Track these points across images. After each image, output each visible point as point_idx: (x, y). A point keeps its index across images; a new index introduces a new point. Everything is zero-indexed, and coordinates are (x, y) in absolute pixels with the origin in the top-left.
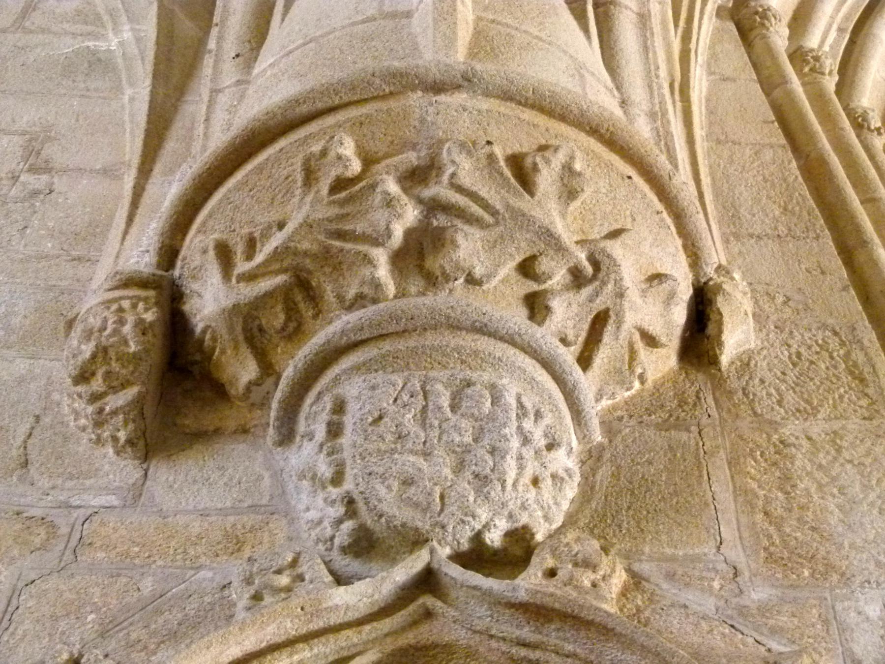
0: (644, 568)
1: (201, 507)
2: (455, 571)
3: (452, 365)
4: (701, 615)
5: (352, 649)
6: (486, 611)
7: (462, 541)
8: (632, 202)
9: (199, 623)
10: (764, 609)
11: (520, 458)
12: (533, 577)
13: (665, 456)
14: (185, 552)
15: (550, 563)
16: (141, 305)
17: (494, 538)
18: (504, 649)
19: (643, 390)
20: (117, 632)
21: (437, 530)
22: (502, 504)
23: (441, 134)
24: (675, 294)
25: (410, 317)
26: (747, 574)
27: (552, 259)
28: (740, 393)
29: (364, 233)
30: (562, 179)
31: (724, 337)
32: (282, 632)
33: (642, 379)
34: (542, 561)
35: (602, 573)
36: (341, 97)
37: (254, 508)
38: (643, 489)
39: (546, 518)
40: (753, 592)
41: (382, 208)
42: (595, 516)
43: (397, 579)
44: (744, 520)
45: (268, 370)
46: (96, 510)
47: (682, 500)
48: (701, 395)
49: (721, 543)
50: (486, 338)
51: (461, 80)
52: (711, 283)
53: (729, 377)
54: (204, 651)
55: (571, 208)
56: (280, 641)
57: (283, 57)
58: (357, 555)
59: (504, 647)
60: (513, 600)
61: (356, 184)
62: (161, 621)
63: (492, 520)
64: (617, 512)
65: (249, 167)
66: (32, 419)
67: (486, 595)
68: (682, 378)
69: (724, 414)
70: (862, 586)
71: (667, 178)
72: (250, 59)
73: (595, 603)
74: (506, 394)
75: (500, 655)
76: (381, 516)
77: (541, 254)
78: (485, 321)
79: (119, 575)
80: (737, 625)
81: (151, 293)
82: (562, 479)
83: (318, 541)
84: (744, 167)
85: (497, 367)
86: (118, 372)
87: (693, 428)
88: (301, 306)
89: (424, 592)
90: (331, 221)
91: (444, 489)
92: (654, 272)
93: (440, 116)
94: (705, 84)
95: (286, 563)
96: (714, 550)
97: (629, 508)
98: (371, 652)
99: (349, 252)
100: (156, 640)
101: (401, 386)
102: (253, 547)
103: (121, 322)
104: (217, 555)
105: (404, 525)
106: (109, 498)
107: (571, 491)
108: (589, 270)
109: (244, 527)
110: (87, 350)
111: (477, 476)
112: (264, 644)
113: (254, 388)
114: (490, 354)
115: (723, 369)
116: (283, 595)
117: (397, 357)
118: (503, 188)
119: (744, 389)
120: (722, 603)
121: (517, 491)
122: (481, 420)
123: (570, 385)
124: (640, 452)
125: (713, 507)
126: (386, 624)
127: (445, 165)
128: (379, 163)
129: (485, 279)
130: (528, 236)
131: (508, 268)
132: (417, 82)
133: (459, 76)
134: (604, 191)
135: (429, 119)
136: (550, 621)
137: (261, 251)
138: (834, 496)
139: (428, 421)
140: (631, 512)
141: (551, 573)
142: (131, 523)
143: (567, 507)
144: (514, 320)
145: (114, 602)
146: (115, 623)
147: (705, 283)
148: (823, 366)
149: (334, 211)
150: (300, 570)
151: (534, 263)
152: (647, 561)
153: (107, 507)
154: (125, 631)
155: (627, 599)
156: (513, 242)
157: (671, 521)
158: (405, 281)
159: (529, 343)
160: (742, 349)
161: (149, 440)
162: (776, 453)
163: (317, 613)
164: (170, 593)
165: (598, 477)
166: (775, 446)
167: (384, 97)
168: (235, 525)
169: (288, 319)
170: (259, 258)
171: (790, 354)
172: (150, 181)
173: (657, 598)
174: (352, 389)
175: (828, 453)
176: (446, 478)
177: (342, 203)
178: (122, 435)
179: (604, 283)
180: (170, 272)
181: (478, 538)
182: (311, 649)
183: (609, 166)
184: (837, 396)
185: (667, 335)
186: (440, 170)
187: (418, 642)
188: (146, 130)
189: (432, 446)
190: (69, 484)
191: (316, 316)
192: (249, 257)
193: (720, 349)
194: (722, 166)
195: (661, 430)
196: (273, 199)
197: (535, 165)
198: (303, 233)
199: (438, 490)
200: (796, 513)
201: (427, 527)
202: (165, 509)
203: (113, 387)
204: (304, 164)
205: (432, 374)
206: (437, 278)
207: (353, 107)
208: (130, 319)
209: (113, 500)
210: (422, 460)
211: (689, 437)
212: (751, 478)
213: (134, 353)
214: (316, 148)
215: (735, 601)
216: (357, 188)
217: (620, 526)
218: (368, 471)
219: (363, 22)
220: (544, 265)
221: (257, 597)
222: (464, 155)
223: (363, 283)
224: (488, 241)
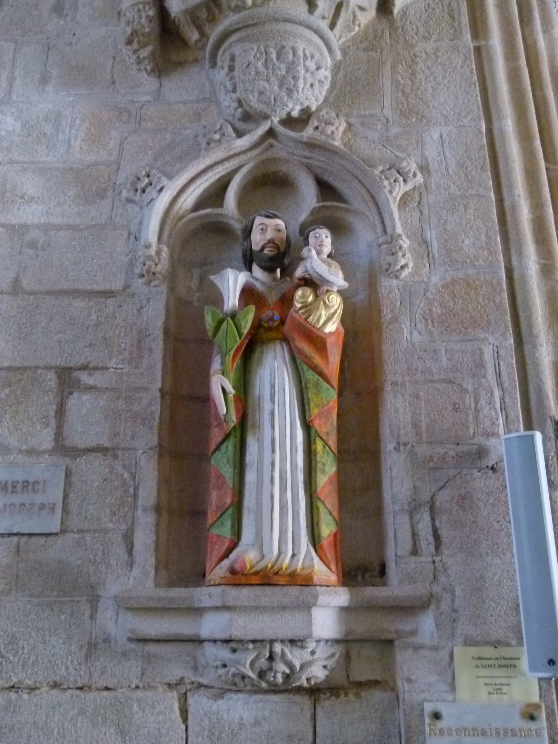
0: (353, 120)
2: (280, 129)
11: (305, 78)
14: (180, 121)
15: (316, 123)
16: (147, 7)
17: (295, 114)
19: (359, 31)
26: (391, 121)
28: (401, 29)
33: (359, 26)
34: (314, 122)
35: (335, 126)
37: (203, 100)
38: (356, 83)
39: (316, 100)
44: (394, 95)
45: (203, 35)
59: (299, 158)
66: (112, 59)
70: (434, 125)
73: (331, 142)
80: (385, 145)
83: (229, 116)
88: (213, 8)
96: (380, 112)
97: (349, 92)
103: (140, 17)
105: (260, 111)
107: (327, 86)
110: (129, 30)
111: (287, 89)
112: (213, 162)
116: (217, 144)
119: (402, 27)
123: (326, 39)
138: (431, 82)
141: (317, 128)
145: (157, 145)
148: (438, 11)
165: (338, 77)
169: (209, 15)
171: (425, 5)
174: (237, 50)
175: (432, 59)
178: (149, 68)
181: (289, 114)
184: (441, 28)
189: (270, 77)
190: (132, 91)
199: (273, 96)
200: (414, 92)
205: (269, 44)
208: (144, 15)
210: (266, 83)
212: (400, 75)
221: (208, 143)
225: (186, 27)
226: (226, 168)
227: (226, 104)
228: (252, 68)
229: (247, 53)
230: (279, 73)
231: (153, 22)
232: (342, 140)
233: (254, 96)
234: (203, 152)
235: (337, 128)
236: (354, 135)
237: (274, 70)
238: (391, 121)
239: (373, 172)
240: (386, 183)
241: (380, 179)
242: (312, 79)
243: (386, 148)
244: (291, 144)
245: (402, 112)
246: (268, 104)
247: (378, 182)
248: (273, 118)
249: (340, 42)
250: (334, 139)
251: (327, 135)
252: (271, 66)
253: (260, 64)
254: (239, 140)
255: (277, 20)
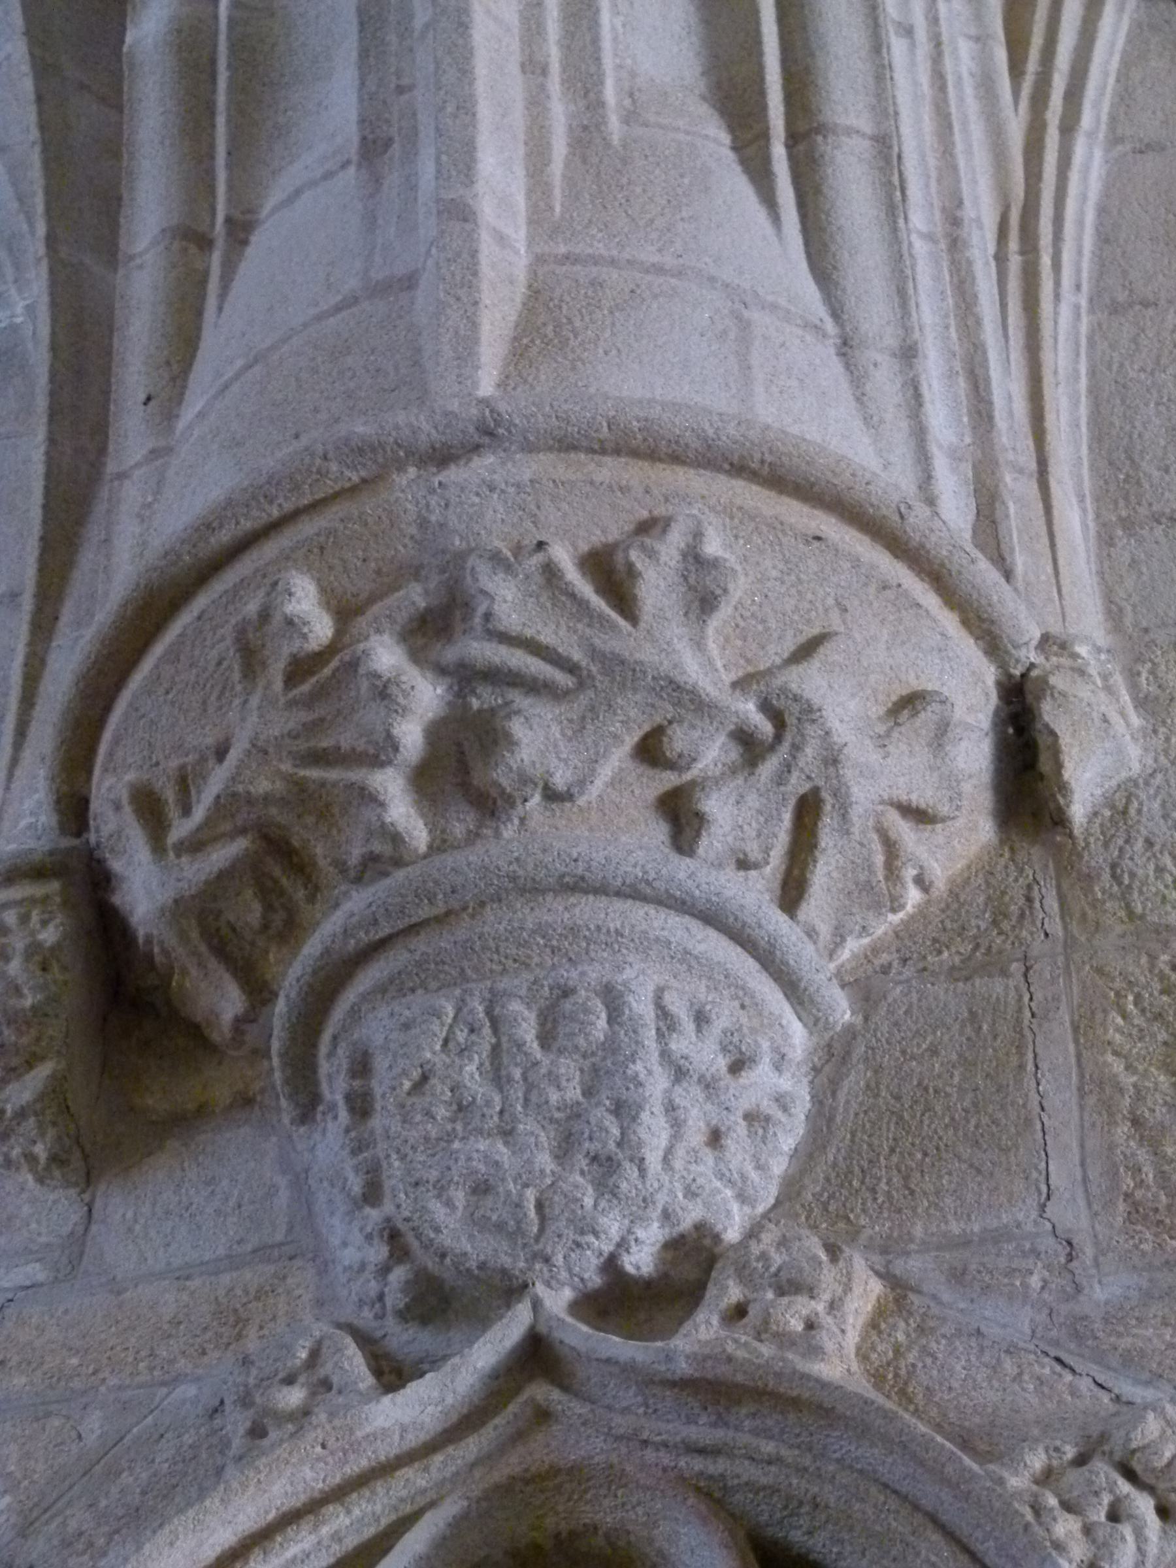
0: (912, 1266)
1: (177, 1262)
3: (536, 960)
4: (1004, 1347)
5: (418, 1499)
6: (636, 1396)
7: (586, 1276)
8: (835, 579)
9: (175, 1486)
10: (1114, 1316)
11: (671, 1108)
12: (703, 1327)
13: (961, 1034)
15: (735, 1293)
16: (35, 916)
18: (666, 1461)
20: (47, 1523)
21: (538, 1266)
22: (644, 1200)
23: (457, 543)
24: (948, 725)
25: (449, 890)
26: (1090, 1251)
27: (693, 727)
28: (1106, 876)
29: (353, 749)
30: (685, 578)
31: (1066, 775)
32: (300, 1488)
33: (920, 881)
35: (827, 1296)
36: (280, 505)
37: (262, 1252)
38: (919, 1109)
39: (742, 1198)
40: (1097, 1287)
41: (374, 699)
42: (833, 1175)
43: (479, 1365)
46: (10, 1296)
47: (985, 1120)
48: (1035, 894)
49: (1048, 1198)
50: (591, 897)
51: (476, 437)
52: (1034, 673)
53: (1088, 844)
54: (166, 1551)
55: (710, 631)
56: (299, 1505)
57: (215, 397)
58: (425, 1320)
59: (666, 1459)
60: (669, 1376)
61: (328, 662)
62: (114, 1490)
63: (629, 1232)
64: (870, 1162)
65: (158, 649)
67: (628, 1370)
68: (1002, 861)
69: (1075, 928)
71: (897, 518)
72: (170, 400)
74: (631, 999)
75: (660, 1473)
76: (443, 1256)
77: (670, 722)
78: (580, 871)
79: (48, 1415)
81: (54, 886)
82: (768, 1119)
83: (361, 1303)
84: (1158, 362)
85: (616, 946)
86: (16, 1044)
87: (1014, 966)
89: (531, 1378)
90: (296, 737)
91: (542, 1192)
92: (904, 693)
93: (451, 509)
94: (1097, 170)
95: (298, 1362)
96: (1034, 1214)
98: (448, 1500)
99: (335, 784)
100: (107, 1529)
101: (451, 1015)
102: (261, 1328)
104: (204, 1353)
105: (482, 1266)
106: (29, 1268)
108: (766, 728)
109: (247, 1292)
111: (595, 1159)
112: (271, 1516)
113: (245, 1027)
114: (598, 928)
115: (1077, 832)
116: (290, 1427)
117: (444, 963)
118: (579, 621)
119: (1114, 866)
120: (1043, 1317)
121: (672, 1169)
122: (593, 1054)
124: (918, 1031)
125: (1038, 1127)
126: (472, 1446)
127: (473, 596)
128: (363, 613)
129: (575, 790)
130: (638, 697)
131: (619, 758)
132: (402, 454)
133: (471, 429)
134: (774, 573)
135: (433, 518)
136: (739, 1402)
137: (198, 801)
139: (503, 1073)
140: (895, 1159)
141: (739, 1312)
142: (66, 1312)
143: (784, 1166)
144: (632, 860)
146: (44, 1505)
147: (1023, 676)
149: (304, 716)
150: (322, 1372)
151: (661, 741)
152: (917, 1252)
153: (28, 1288)
154: (60, 1519)
155: (880, 1332)
156: (615, 714)
157: (964, 1166)
158: (443, 817)
159: (667, 891)
160: (1114, 783)
161: (88, 1147)
162: (1162, 992)
163: (354, 1447)
164: (129, 1437)
165: (842, 1096)
166: (1162, 977)
167: (352, 491)
168: (232, 1289)
169: (268, 908)
170: (199, 814)
172: (54, 644)
173: (932, 1324)
176: (542, 1171)
177: (309, 702)
179: (796, 748)
180: (83, 839)
181: (611, 1265)
182: (349, 1512)
183: (777, 526)
185: (951, 799)
186: (467, 607)
187: (527, 1470)
188: (42, 539)
191: (311, 899)
192: (187, 811)
193: (1064, 796)
194: (1115, 367)
195: (957, 980)
196: (204, 703)
197: (630, 566)
198: (254, 766)
199: (531, 1195)
201: (522, 1264)
202: (119, 1277)
203: (14, 1069)
204: (238, 640)
205: (504, 984)
206: (495, 803)
207: (305, 518)
209: (36, 1272)
210: (500, 1146)
211: (1007, 987)
212: (1116, 1053)
213: (33, 1007)
214: (252, 608)
215: (1064, 1309)
216: (327, 671)
217: (873, 1191)
218: (413, 1180)
219: (338, 309)
220: (678, 741)
221: (257, 1432)
222: (502, 575)
223: (370, 834)
224: (571, 721)
225: (194, 972)
226: (336, 1537)
227: (350, 1256)
228: (439, 1088)
229: (415, 1031)
230: (554, 1097)
231: (55, 968)
232: (863, 1355)
233: (449, 1204)
234: (230, 1471)
235: (833, 1306)
236: (921, 1330)
237: (530, 1087)
238: (1089, 1251)
239: (1001, 1481)
240: (1066, 1527)
241: (1037, 1509)
242: (708, 1106)
243: (1073, 1371)
244: (629, 1397)
245: (1136, 1205)
246: (511, 1232)
247: (1027, 1527)
248: (540, 1289)
249: (845, 954)
250: (815, 1351)
251: (784, 1339)
252: (517, 1074)
253: (471, 1072)
254: (387, 1400)
255: (532, 890)
